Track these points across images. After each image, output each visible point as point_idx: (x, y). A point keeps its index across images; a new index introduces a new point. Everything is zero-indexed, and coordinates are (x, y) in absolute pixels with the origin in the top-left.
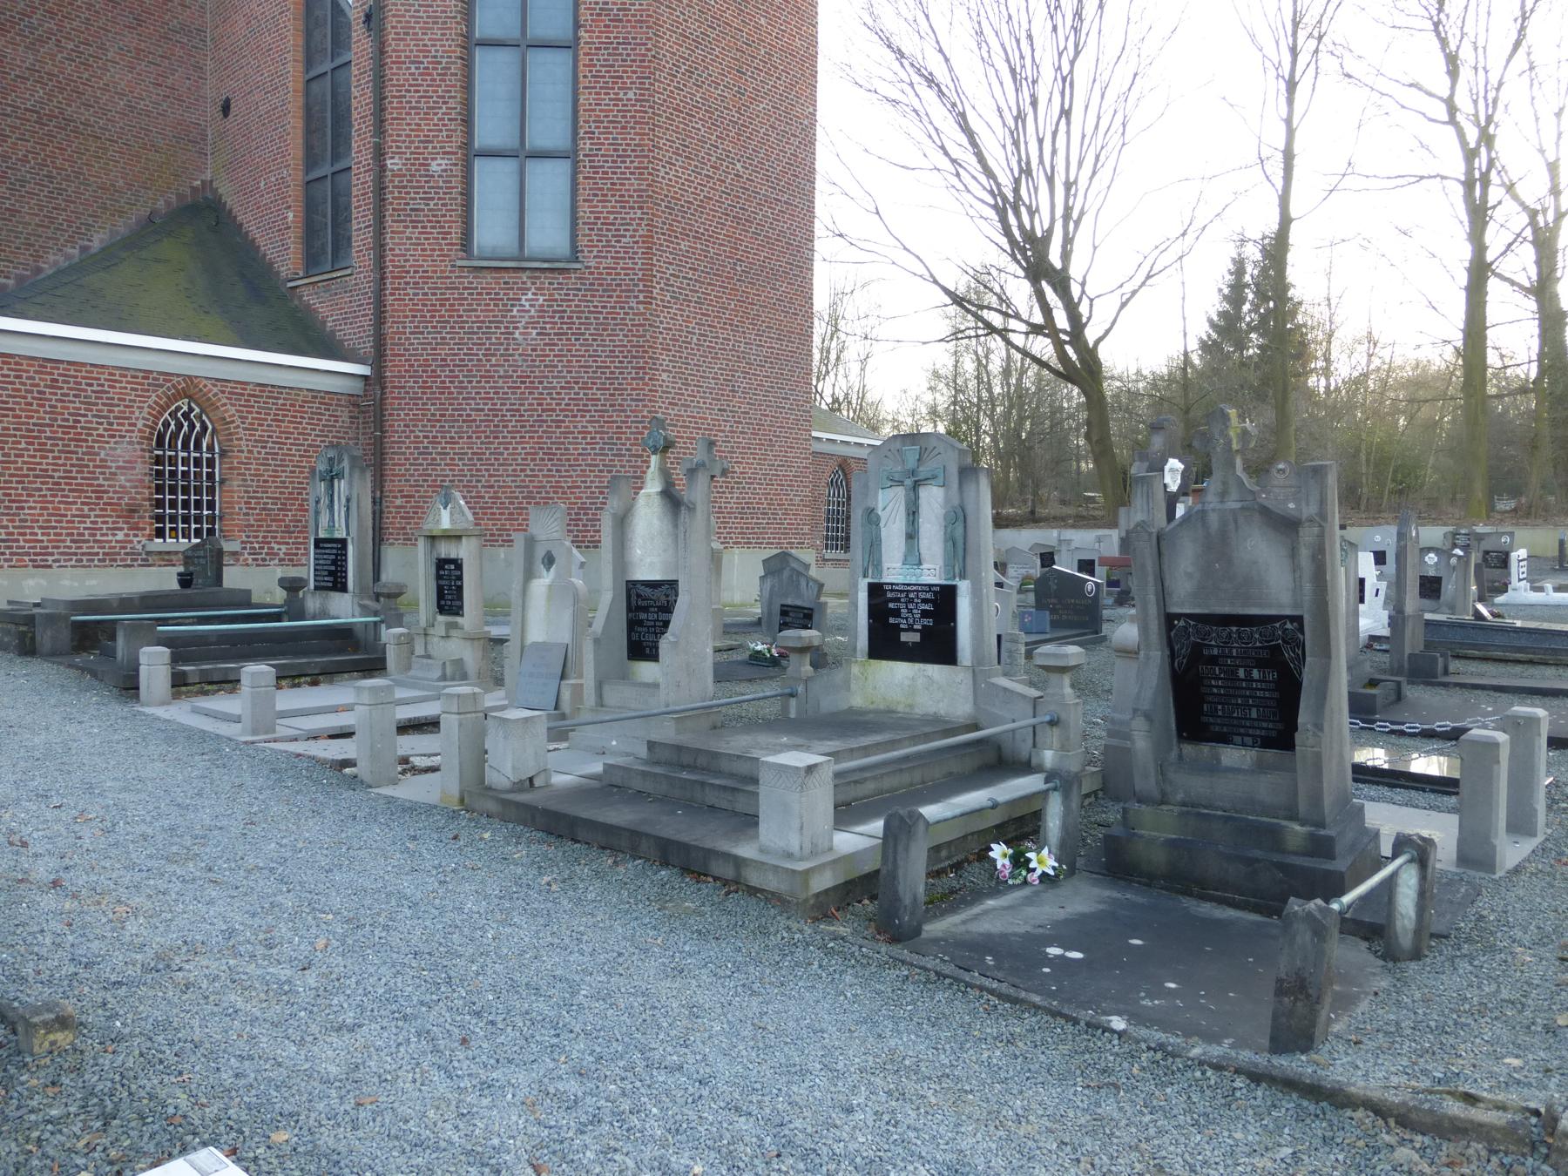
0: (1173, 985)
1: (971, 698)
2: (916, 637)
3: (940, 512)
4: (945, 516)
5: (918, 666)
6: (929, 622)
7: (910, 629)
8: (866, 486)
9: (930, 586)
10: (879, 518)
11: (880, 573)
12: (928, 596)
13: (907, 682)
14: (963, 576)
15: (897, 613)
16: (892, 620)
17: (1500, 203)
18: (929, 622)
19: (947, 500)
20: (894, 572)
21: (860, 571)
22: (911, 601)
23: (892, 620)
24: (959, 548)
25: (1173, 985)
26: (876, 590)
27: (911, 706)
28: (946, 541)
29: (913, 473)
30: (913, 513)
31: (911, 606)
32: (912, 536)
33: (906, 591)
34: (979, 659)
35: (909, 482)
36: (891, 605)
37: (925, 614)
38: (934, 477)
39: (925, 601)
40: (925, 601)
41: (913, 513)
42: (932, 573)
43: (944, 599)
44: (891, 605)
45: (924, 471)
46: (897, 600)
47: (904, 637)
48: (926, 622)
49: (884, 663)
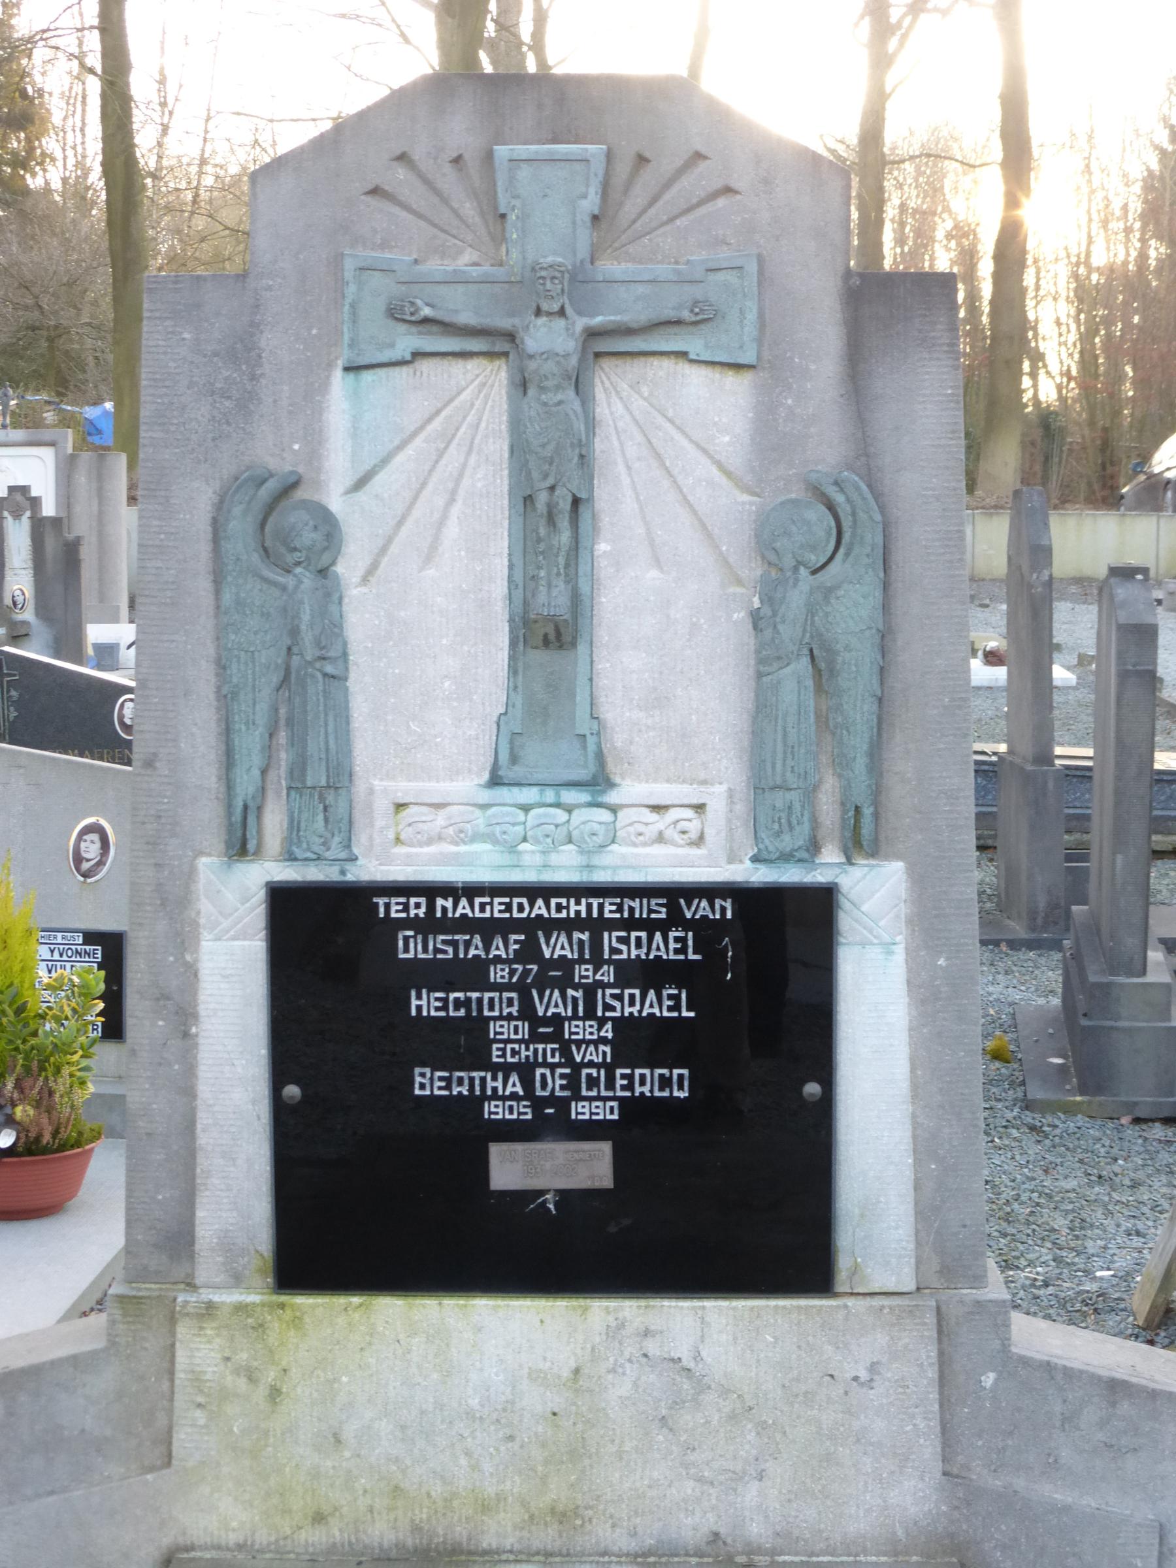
0: (551, 1111)
1: (928, 1450)
2: (590, 1166)
3: (731, 506)
4: (766, 540)
5: (602, 1313)
6: (663, 1083)
7: (551, 1122)
8: (243, 351)
9: (675, 895)
10: (329, 529)
11: (345, 829)
12: (664, 947)
13: (535, 1400)
14: (859, 843)
15: (465, 1043)
16: (428, 1083)
17: (856, 25)
18: (663, 1083)
19: (771, 437)
20: (430, 813)
21: (205, 818)
22: (559, 975)
23: (428, 1083)
24: (818, 673)
25: (551, 1111)
26: (328, 945)
27: (562, 1516)
28: (766, 661)
29: (579, 283)
30: (553, 507)
31: (550, 1004)
32: (549, 634)
33: (528, 922)
34: (946, 1257)
35: (550, 339)
36: (425, 1004)
37: (637, 1042)
38: (700, 318)
39: (650, 975)
40: (650, 975)
41: (553, 507)
42: (676, 821)
43: (756, 970)
44: (425, 1004)
45: (632, 281)
46: (473, 974)
47: (509, 1167)
48: (647, 1082)
49: (390, 1309)
